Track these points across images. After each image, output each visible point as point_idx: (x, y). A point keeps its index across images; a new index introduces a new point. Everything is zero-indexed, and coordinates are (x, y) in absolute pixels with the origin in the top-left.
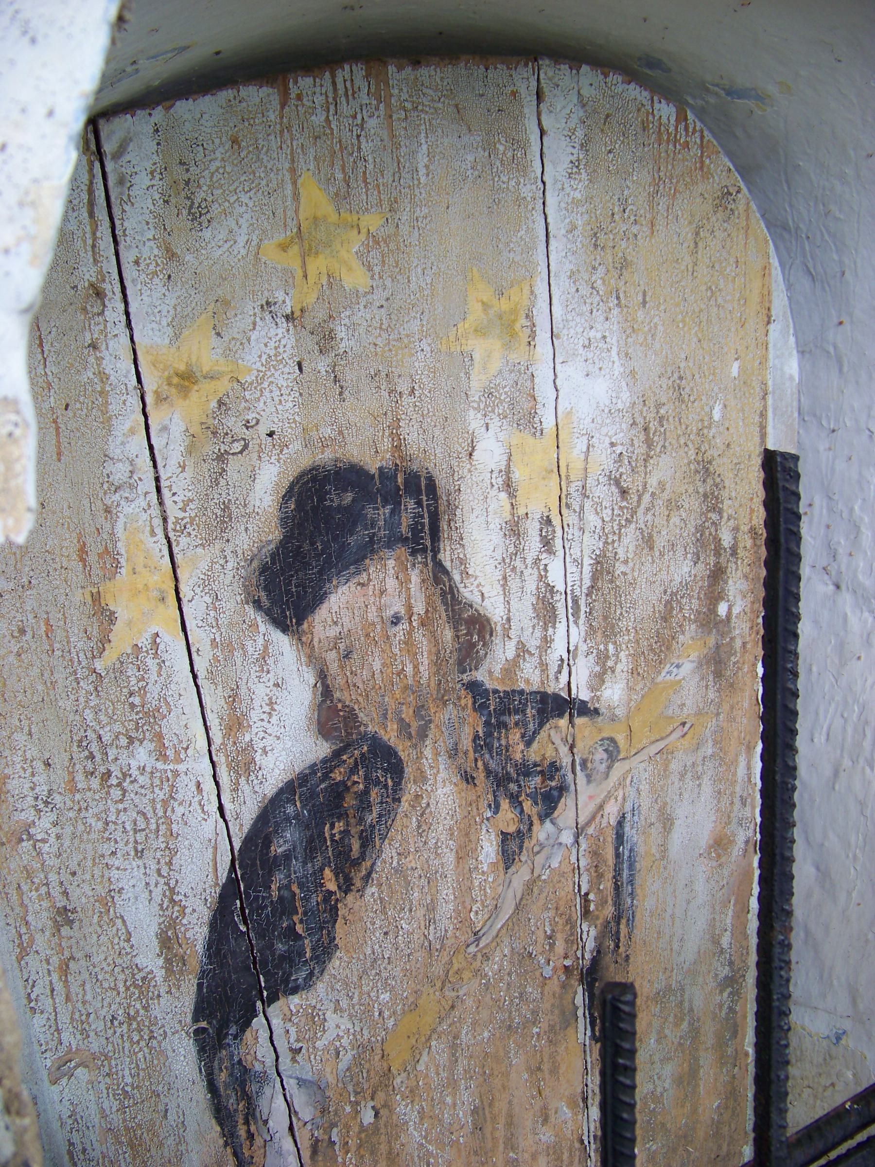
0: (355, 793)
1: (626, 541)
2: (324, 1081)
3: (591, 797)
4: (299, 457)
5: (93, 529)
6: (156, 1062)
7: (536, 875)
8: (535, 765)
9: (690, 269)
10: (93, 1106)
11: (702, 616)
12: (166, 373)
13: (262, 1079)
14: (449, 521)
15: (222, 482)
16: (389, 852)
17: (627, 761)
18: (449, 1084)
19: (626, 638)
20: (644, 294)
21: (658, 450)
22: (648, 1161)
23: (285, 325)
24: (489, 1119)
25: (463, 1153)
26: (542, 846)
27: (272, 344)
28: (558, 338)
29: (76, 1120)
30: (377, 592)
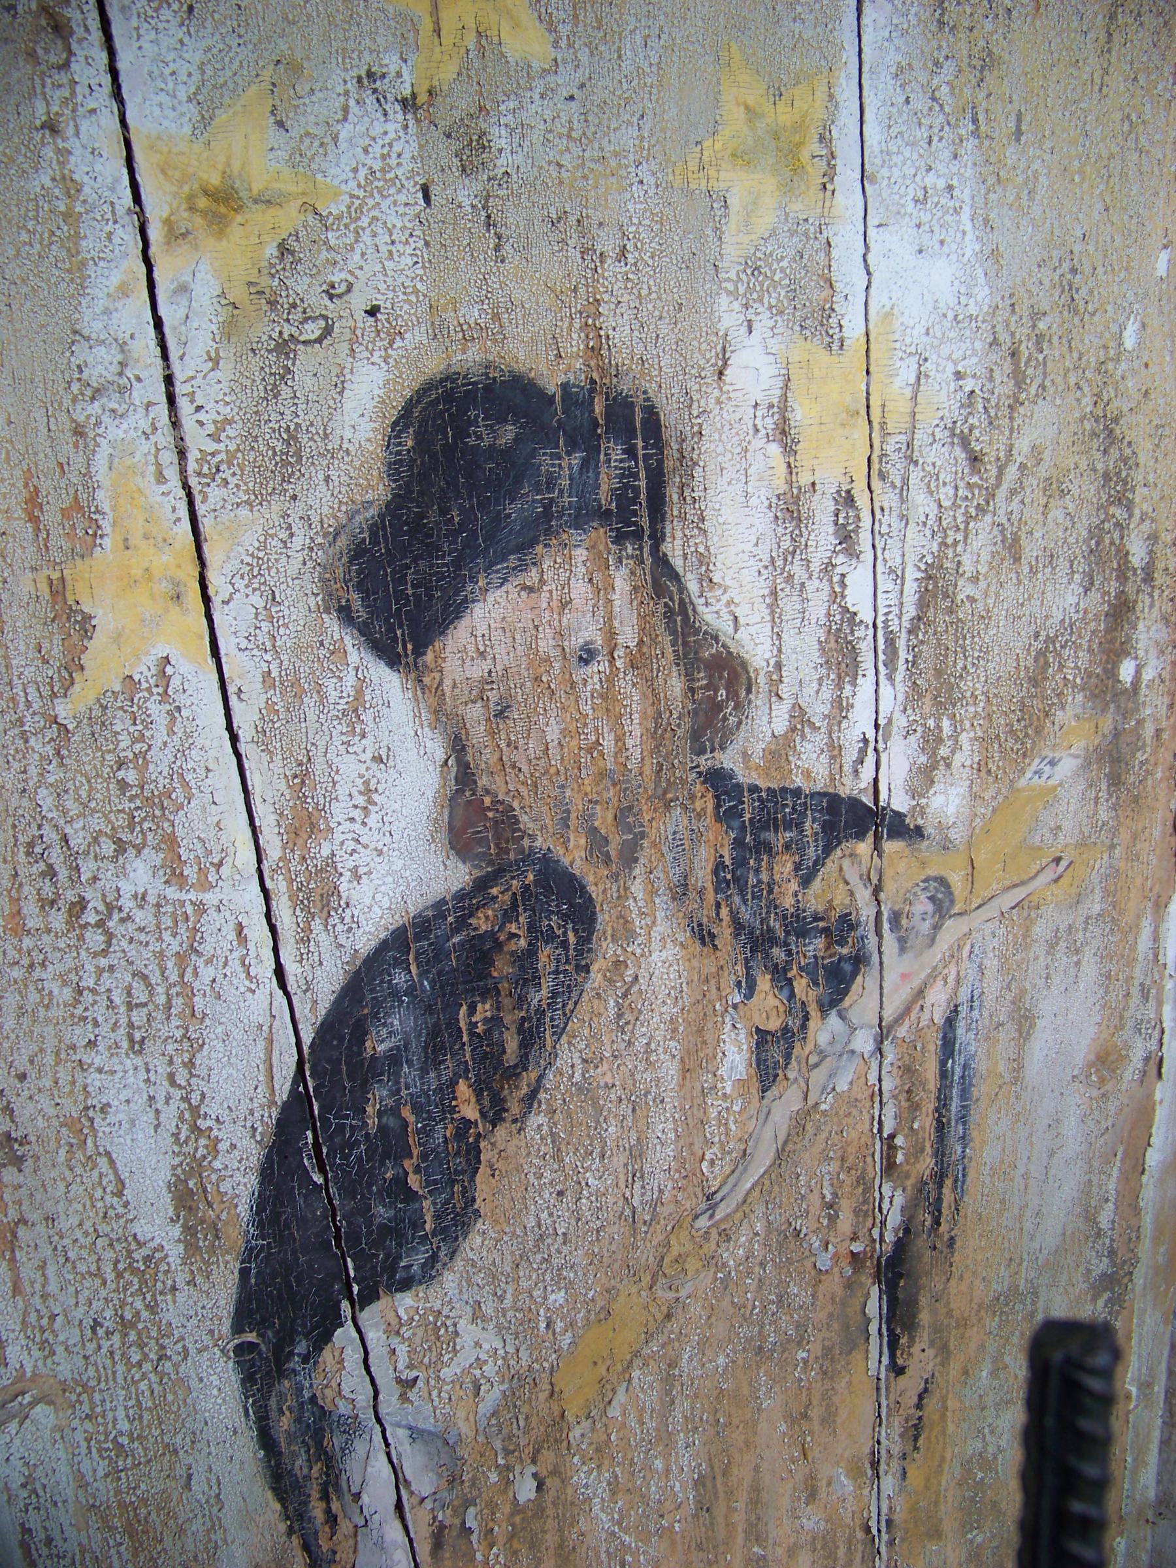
0: (512, 953)
1: (975, 543)
2: (454, 1432)
3: (904, 976)
4: (422, 357)
5: (53, 464)
6: (170, 1397)
7: (811, 1102)
8: (816, 918)
9: (1097, 81)
10: (63, 1469)
11: (1094, 680)
12: (186, 188)
13: (351, 1427)
14: (682, 487)
15: (286, 392)
16: (568, 1057)
17: (966, 918)
18: (659, 1439)
19: (971, 709)
20: (1019, 120)
21: (1033, 391)
22: (969, 1560)
23: (400, 117)
24: (721, 1494)
25: (680, 1548)
26: (823, 1055)
27: (376, 150)
28: (873, 181)
29: (34, 1491)
30: (555, 604)
